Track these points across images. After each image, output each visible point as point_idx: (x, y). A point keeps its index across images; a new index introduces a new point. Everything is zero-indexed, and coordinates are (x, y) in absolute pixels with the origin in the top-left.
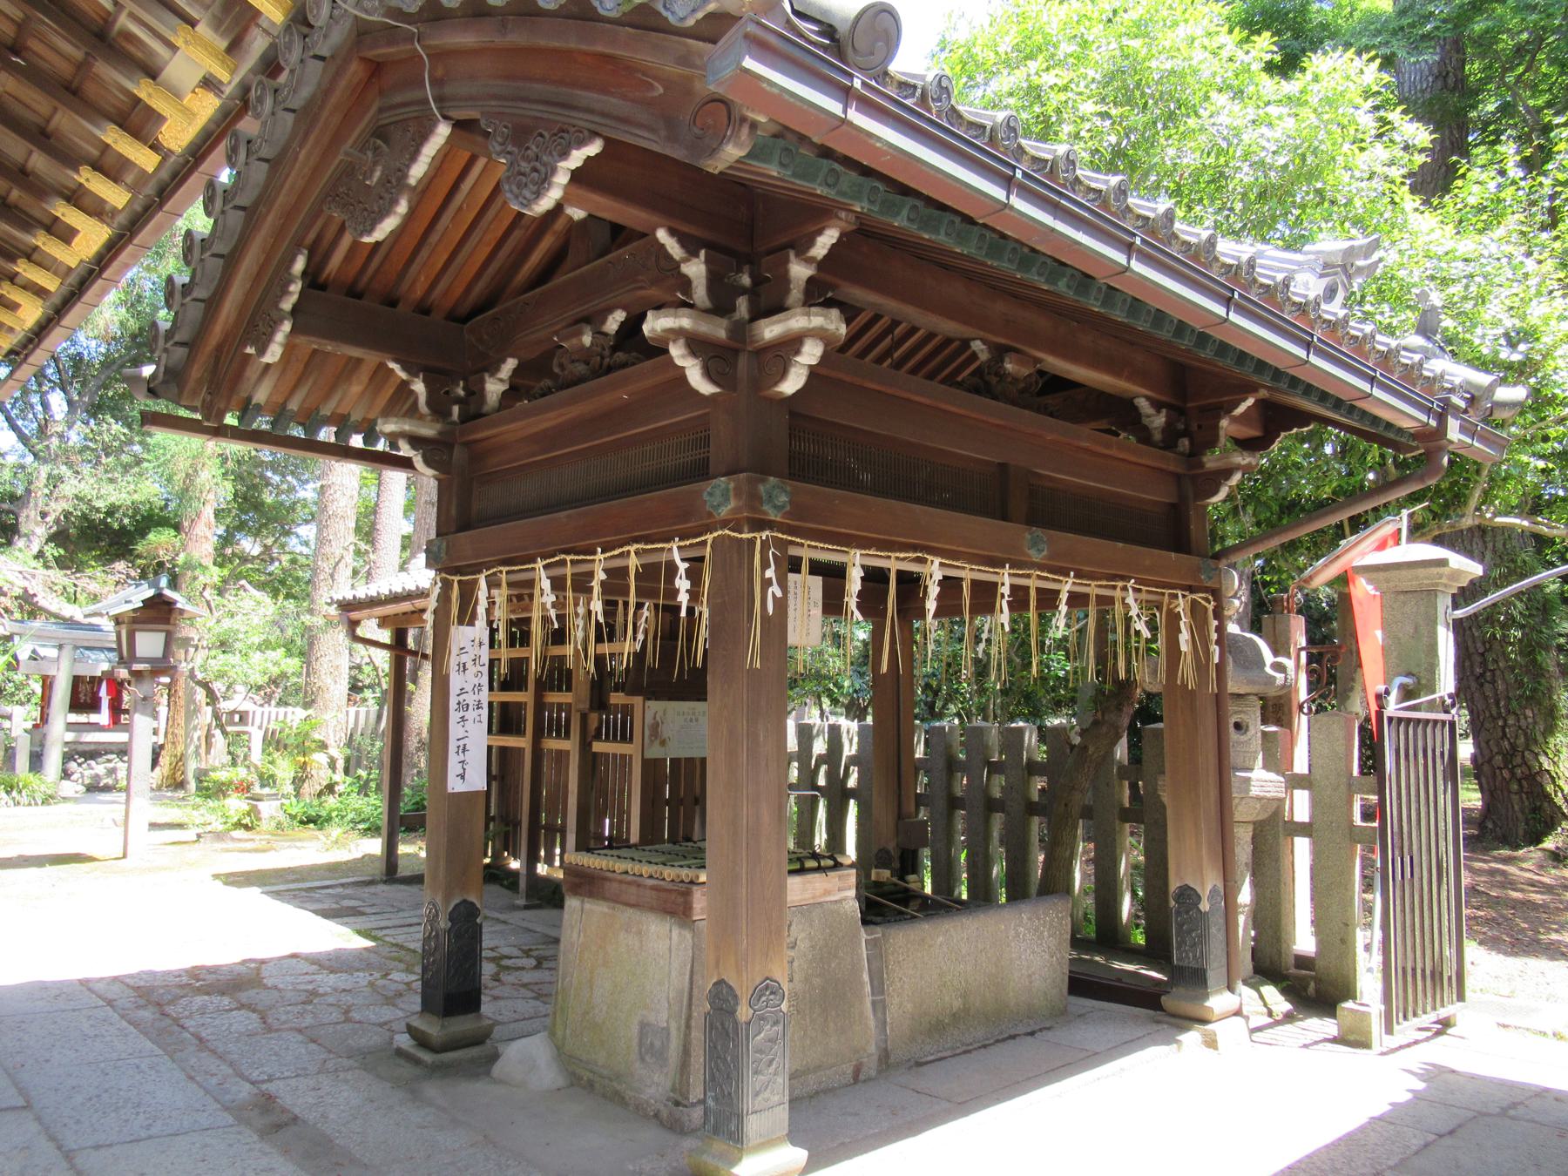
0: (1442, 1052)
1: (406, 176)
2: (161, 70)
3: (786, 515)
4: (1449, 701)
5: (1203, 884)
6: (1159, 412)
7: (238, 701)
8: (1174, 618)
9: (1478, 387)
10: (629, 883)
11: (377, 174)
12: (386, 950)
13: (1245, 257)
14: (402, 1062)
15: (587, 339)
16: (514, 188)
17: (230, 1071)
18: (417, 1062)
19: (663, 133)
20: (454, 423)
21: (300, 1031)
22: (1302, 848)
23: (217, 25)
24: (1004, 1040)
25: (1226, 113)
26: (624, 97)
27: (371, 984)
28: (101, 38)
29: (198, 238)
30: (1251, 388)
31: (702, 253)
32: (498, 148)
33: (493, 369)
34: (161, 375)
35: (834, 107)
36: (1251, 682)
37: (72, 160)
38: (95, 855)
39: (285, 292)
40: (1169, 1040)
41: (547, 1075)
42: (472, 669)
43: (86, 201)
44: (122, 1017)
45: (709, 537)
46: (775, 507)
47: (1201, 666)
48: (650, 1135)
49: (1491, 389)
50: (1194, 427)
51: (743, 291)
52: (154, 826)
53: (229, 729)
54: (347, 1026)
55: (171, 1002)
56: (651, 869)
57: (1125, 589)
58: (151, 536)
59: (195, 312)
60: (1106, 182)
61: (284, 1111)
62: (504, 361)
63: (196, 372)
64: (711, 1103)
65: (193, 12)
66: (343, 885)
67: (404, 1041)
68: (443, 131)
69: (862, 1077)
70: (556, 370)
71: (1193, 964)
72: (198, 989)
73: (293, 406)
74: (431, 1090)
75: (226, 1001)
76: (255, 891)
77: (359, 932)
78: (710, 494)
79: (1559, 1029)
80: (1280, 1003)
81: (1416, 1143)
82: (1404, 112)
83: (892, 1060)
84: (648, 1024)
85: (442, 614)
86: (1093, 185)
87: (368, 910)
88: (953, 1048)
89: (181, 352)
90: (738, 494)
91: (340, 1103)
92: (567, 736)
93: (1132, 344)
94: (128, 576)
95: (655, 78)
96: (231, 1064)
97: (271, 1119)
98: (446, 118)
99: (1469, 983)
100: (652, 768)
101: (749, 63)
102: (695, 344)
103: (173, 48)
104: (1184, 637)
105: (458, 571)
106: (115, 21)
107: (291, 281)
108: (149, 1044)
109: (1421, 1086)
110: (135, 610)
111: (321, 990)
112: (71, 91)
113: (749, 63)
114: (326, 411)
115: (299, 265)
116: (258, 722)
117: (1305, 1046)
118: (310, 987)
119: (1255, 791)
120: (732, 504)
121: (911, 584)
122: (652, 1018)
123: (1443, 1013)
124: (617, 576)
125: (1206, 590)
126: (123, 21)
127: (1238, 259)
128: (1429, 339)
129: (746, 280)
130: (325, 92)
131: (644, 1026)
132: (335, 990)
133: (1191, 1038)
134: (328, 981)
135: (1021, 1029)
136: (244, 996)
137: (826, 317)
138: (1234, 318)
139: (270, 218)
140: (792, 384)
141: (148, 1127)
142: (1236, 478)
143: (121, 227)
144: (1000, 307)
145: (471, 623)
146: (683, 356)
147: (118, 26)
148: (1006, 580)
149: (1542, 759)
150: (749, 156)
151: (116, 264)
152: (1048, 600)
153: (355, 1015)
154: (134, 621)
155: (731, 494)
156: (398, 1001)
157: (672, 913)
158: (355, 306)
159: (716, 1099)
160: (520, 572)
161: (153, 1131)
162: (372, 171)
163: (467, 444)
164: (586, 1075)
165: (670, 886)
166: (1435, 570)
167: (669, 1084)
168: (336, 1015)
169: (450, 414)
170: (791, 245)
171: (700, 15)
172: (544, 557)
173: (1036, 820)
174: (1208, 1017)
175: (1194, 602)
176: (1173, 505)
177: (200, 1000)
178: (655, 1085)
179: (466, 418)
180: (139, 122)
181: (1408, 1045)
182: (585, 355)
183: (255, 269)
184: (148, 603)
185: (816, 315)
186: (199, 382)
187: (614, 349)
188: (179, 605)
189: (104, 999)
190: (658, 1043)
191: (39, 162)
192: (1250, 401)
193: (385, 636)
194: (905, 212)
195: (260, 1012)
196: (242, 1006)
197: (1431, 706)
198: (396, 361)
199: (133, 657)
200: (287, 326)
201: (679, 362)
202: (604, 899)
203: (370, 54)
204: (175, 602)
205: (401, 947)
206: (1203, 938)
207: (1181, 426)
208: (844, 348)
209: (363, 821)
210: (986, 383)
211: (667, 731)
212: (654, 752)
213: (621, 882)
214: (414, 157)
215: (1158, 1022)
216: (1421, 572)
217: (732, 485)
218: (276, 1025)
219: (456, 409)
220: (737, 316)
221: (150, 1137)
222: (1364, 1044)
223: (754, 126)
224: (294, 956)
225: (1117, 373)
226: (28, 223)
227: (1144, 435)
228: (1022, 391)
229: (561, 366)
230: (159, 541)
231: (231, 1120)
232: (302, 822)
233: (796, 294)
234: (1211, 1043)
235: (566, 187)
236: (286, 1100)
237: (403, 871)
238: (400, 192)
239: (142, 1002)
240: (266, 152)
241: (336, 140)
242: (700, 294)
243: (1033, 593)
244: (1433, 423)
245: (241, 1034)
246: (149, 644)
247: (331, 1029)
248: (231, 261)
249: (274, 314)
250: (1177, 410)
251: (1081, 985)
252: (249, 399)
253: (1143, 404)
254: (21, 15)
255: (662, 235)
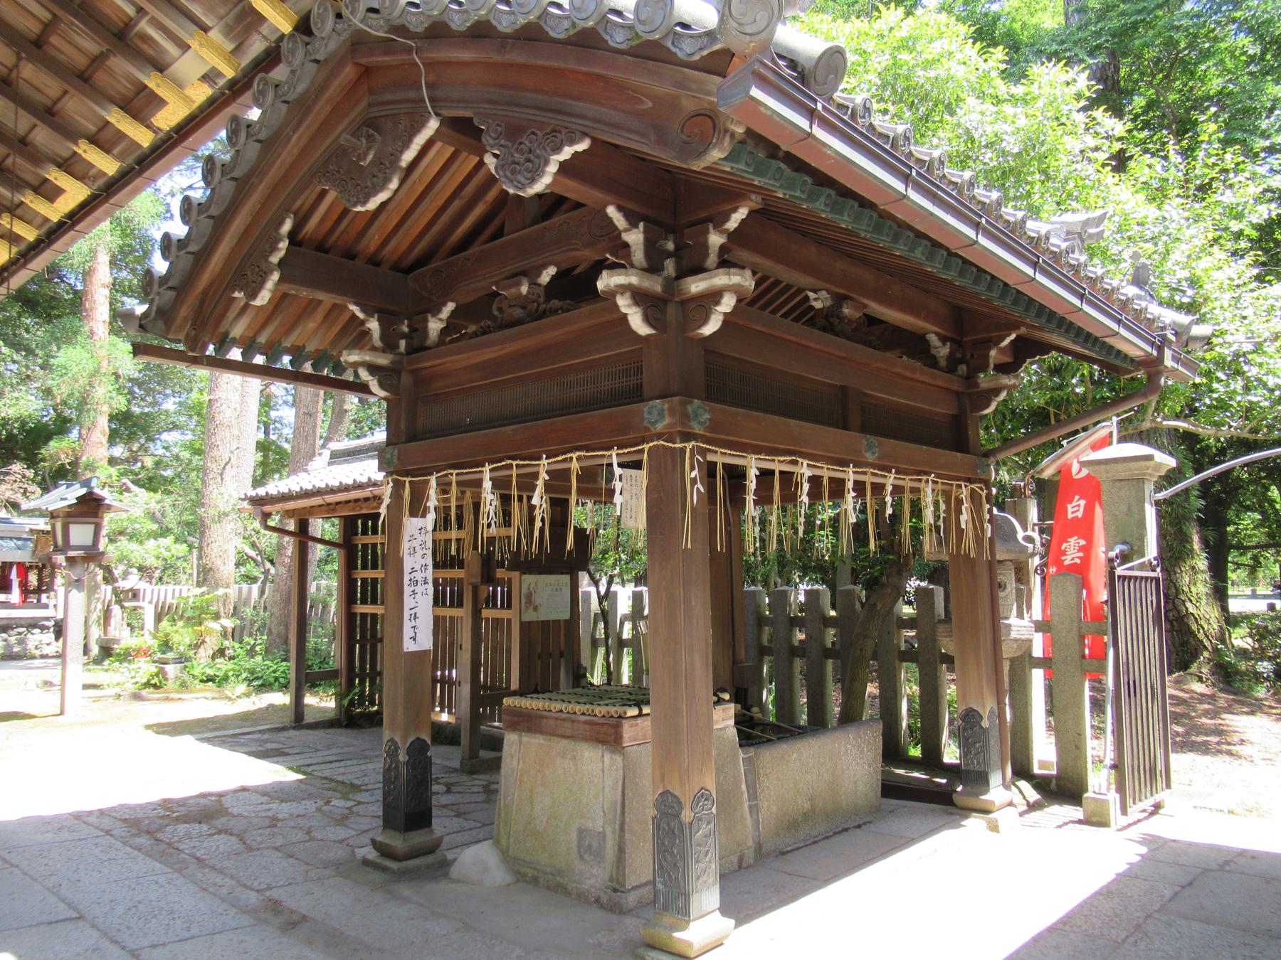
0: (1156, 827)
1: (399, 159)
2: (169, 65)
3: (707, 429)
4: (1155, 563)
5: (984, 707)
6: (944, 345)
7: (133, 581)
8: (959, 502)
9: (1181, 326)
10: (564, 720)
11: (370, 157)
12: (319, 783)
13: (1043, 232)
14: (368, 869)
15: (524, 289)
16: (508, 174)
17: (233, 883)
18: (384, 869)
19: (653, 137)
20: (401, 354)
21: (277, 849)
22: (1037, 678)
23: (228, 32)
24: (840, 832)
25: (972, 113)
26: (614, 108)
27: (319, 810)
28: (121, 37)
29: (195, 203)
30: (1014, 326)
31: (641, 225)
32: (491, 142)
33: (436, 311)
34: (153, 314)
35: (803, 123)
36: (1009, 551)
37: (72, 134)
38: (32, 713)
39: (274, 249)
40: (959, 826)
41: (498, 874)
42: (420, 553)
43: (78, 168)
44: (124, 843)
45: (646, 447)
46: (700, 423)
47: (979, 540)
48: (596, 916)
49: (1189, 327)
50: (968, 356)
51: (669, 255)
52: (86, 687)
53: (126, 604)
54: (314, 844)
55: (160, 829)
56: (583, 708)
57: (927, 481)
58: (52, 444)
59: (186, 262)
60: (961, 177)
61: (292, 912)
62: (444, 304)
63: (184, 311)
64: (660, 886)
65: (208, 22)
66: (260, 732)
67: (371, 854)
68: (433, 125)
69: (744, 865)
70: (496, 313)
71: (977, 768)
72: (177, 819)
73: (262, 339)
74: (405, 890)
75: (205, 827)
76: (188, 740)
77: (291, 768)
78: (650, 413)
79: (1232, 807)
80: (1033, 795)
81: (1168, 893)
82: (1105, 111)
83: (764, 850)
84: (586, 830)
85: (396, 507)
86: (953, 179)
87: (291, 751)
88: (804, 840)
89: (171, 295)
90: (672, 412)
91: (335, 902)
92: (509, 606)
93: (927, 292)
94: (24, 476)
95: (645, 96)
96: (232, 877)
97: (281, 917)
98: (437, 114)
99: (1173, 777)
100: (526, 627)
101: (756, 92)
102: (639, 296)
103: (185, 47)
104: (964, 517)
105: (408, 473)
106: (136, 24)
107: (279, 240)
108: (158, 865)
109: (1144, 850)
110: (70, 506)
111: (280, 816)
112: (83, 78)
113: (756, 92)
114: (287, 343)
115: (287, 226)
116: (148, 597)
117: (1060, 827)
118: (270, 814)
119: (1014, 635)
120: (667, 420)
121: (736, 476)
122: (589, 825)
123: (1157, 798)
124: (559, 479)
125: (980, 481)
126: (144, 26)
127: (1038, 232)
128: (1141, 288)
129: (670, 246)
130: (319, 89)
131: (581, 831)
132: (291, 815)
133: (974, 823)
134: (284, 809)
135: (850, 824)
136: (220, 822)
137: (742, 276)
138: (1040, 278)
139: (260, 188)
140: (711, 327)
141: (188, 929)
142: (1003, 395)
143: (99, 189)
144: (840, 265)
145: (424, 516)
146: (629, 306)
147: (137, 29)
148: (850, 476)
149: (1188, 604)
150: (725, 159)
151: (89, 219)
152: (837, 489)
153: (314, 834)
154: (69, 515)
155: (666, 412)
156: (347, 822)
157: (604, 742)
158: (328, 260)
159: (664, 883)
160: (468, 474)
161: (194, 931)
162: (366, 155)
163: (413, 371)
164: (531, 873)
165: (602, 721)
166: (1144, 463)
167: (607, 877)
168: (301, 836)
169: (398, 347)
170: (709, 219)
171: (705, 53)
172: (491, 462)
173: (830, 662)
174: (991, 808)
175: (972, 490)
176: (955, 416)
177: (182, 828)
178: (594, 877)
179: (411, 351)
180: (140, 104)
181: (1135, 823)
182: (524, 302)
183: (243, 227)
184: (81, 500)
185: (735, 274)
186: (185, 320)
187: (548, 300)
188: (107, 502)
189: (102, 830)
190: (595, 845)
191: (43, 137)
192: (1013, 336)
193: (291, 525)
194: (822, 199)
195: (237, 835)
196: (220, 832)
197: (1142, 567)
198: (357, 304)
199: (67, 545)
200: (276, 276)
201: (624, 310)
202: (541, 733)
203: (363, 61)
204: (103, 499)
205: (331, 780)
206: (985, 748)
207: (959, 355)
208: (752, 303)
209: (257, 678)
210: (827, 322)
211: (538, 599)
212: (530, 616)
213: (556, 719)
214: (406, 144)
215: (952, 814)
216: (1133, 465)
217: (666, 406)
218: (255, 845)
219: (403, 343)
220: (665, 273)
221: (192, 937)
222: (1103, 823)
223: (733, 135)
224: (244, 789)
225: (916, 314)
226: (18, 184)
227: (932, 362)
228: (856, 329)
229: (500, 309)
230: (58, 449)
231: (252, 921)
232: (202, 681)
233: (712, 259)
234: (994, 827)
235: (556, 174)
236: (290, 903)
237: (308, 719)
238: (393, 173)
239: (134, 831)
240: (262, 136)
241: (324, 128)
242: (638, 255)
243: (869, 487)
244: (1155, 353)
245: (229, 853)
246: (80, 534)
247: (301, 846)
248: (221, 223)
249: (263, 265)
250: (957, 343)
251: (892, 789)
252: (226, 334)
253: (933, 339)
254: (49, 16)
255: (611, 211)
